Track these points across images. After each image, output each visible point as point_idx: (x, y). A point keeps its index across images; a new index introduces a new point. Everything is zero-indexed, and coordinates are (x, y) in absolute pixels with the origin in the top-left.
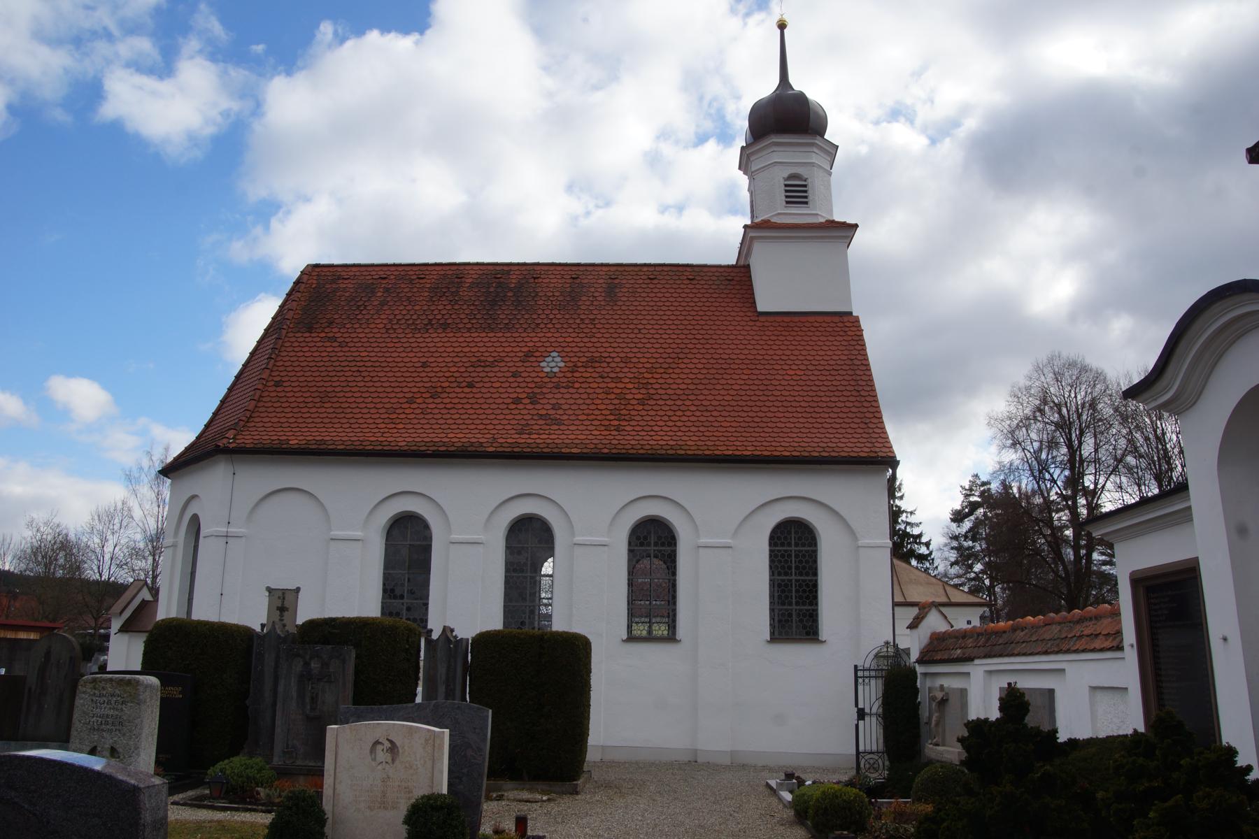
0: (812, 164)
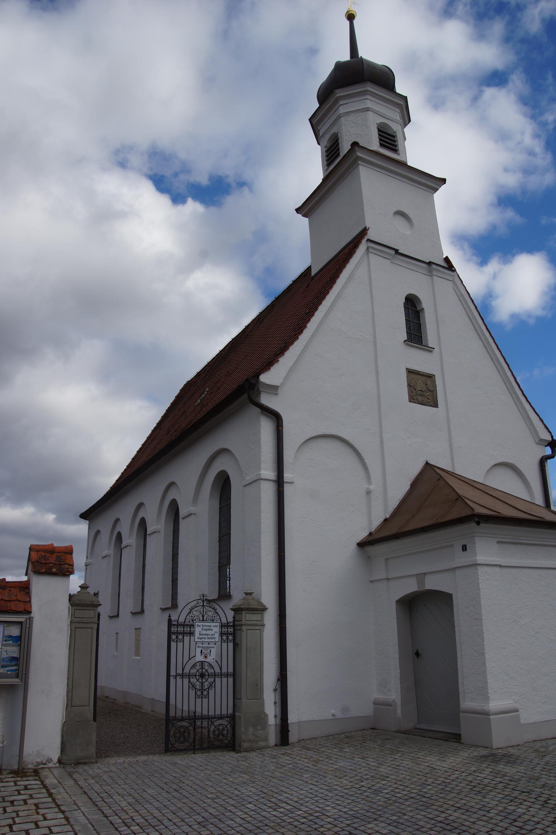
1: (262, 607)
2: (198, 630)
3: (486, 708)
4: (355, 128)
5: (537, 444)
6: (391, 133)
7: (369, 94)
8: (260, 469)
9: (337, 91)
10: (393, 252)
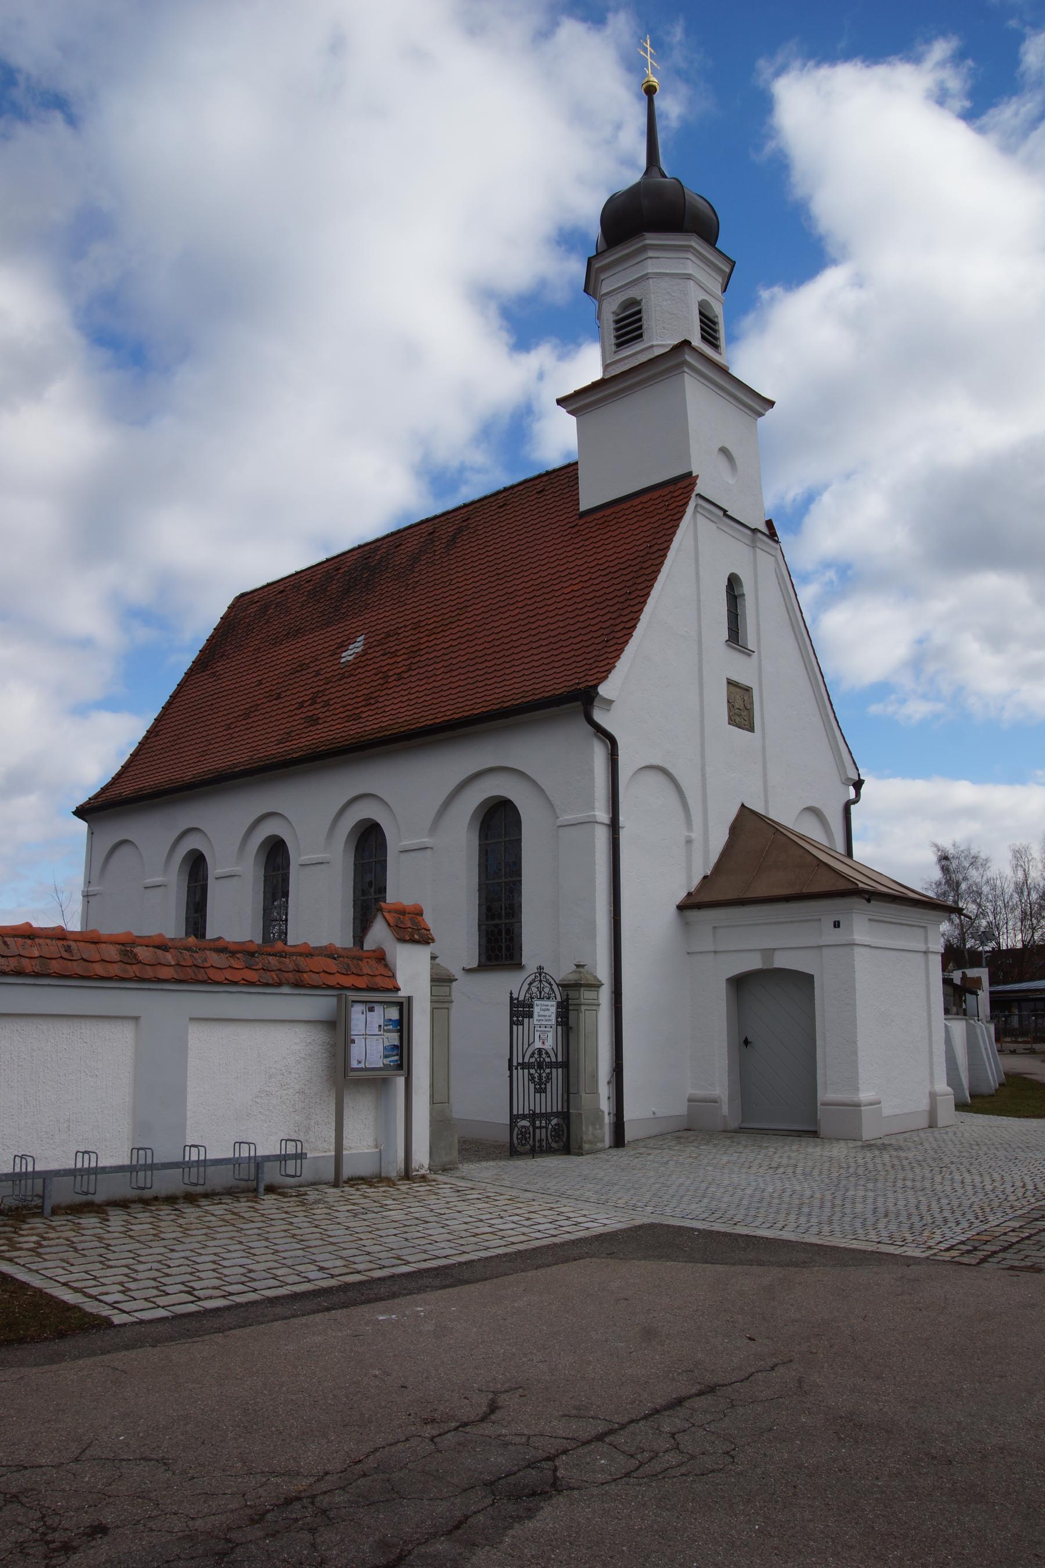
0: (646, 277)
1: (596, 983)
2: (537, 1010)
3: (855, 1099)
4: (669, 302)
5: (843, 783)
6: (711, 317)
7: (692, 253)
8: (593, 809)
9: (647, 235)
10: (721, 513)
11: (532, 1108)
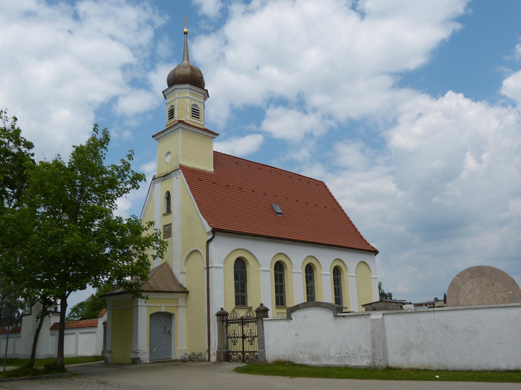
9: (175, 85)
11: (248, 350)
